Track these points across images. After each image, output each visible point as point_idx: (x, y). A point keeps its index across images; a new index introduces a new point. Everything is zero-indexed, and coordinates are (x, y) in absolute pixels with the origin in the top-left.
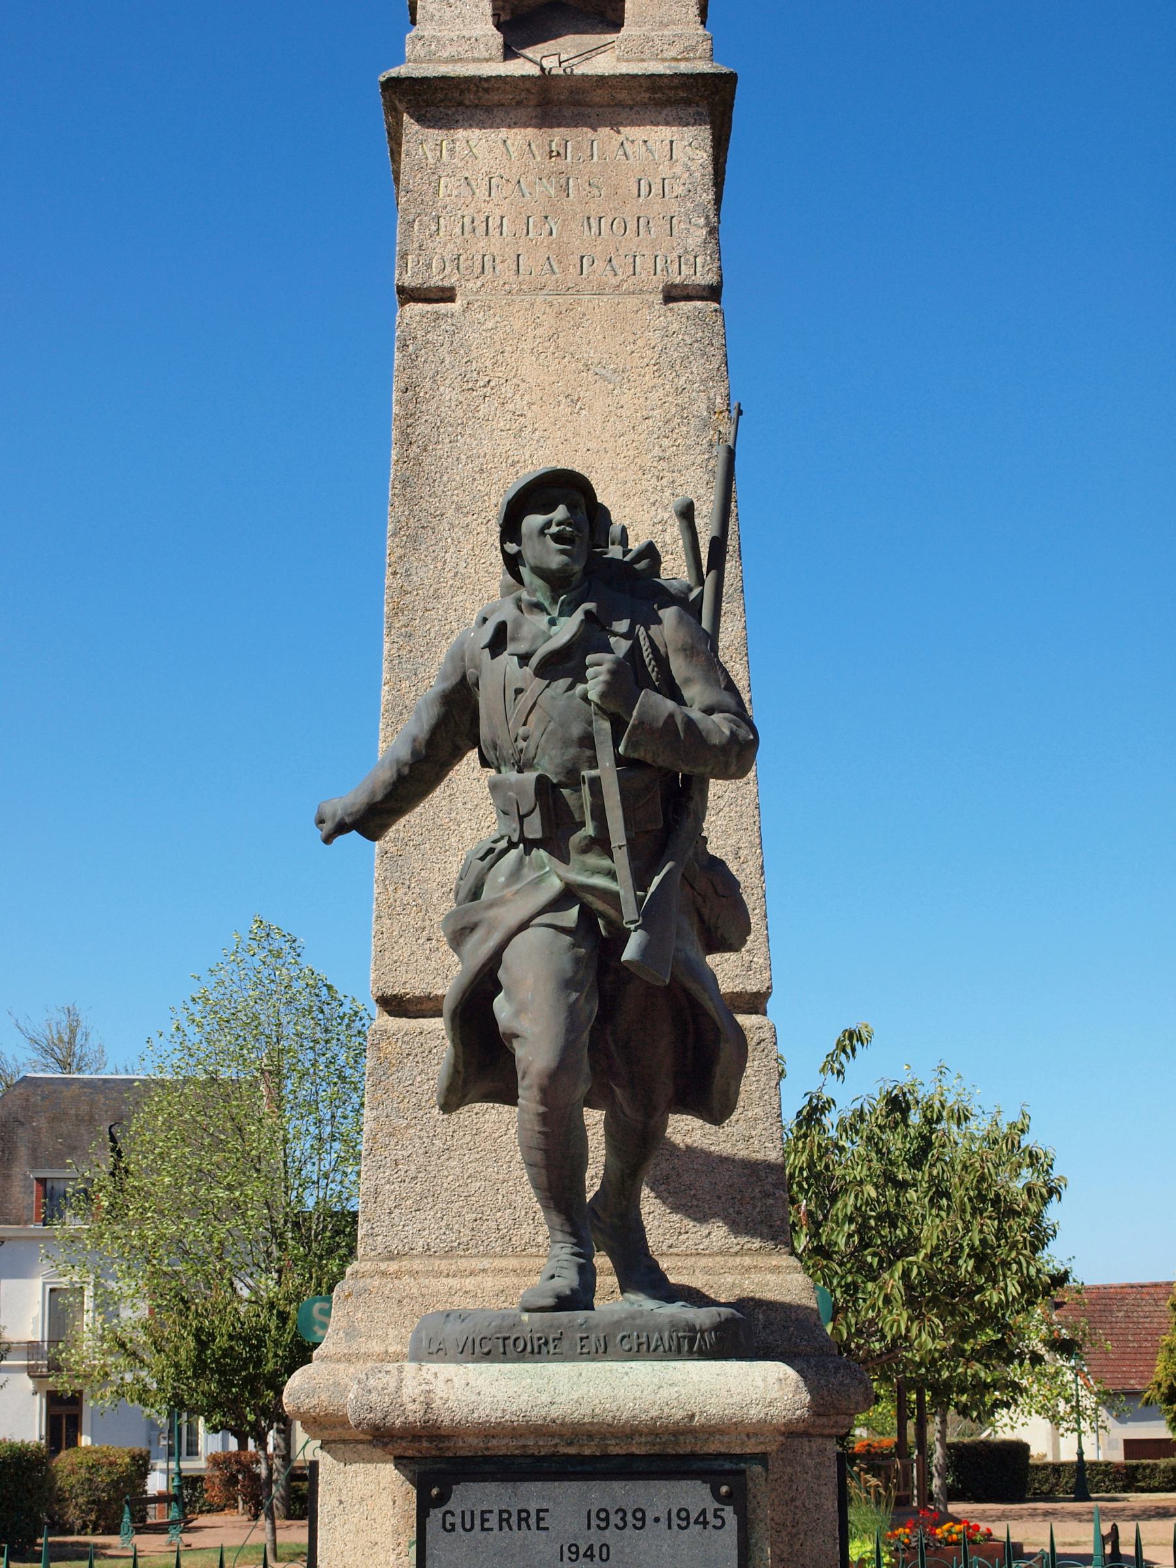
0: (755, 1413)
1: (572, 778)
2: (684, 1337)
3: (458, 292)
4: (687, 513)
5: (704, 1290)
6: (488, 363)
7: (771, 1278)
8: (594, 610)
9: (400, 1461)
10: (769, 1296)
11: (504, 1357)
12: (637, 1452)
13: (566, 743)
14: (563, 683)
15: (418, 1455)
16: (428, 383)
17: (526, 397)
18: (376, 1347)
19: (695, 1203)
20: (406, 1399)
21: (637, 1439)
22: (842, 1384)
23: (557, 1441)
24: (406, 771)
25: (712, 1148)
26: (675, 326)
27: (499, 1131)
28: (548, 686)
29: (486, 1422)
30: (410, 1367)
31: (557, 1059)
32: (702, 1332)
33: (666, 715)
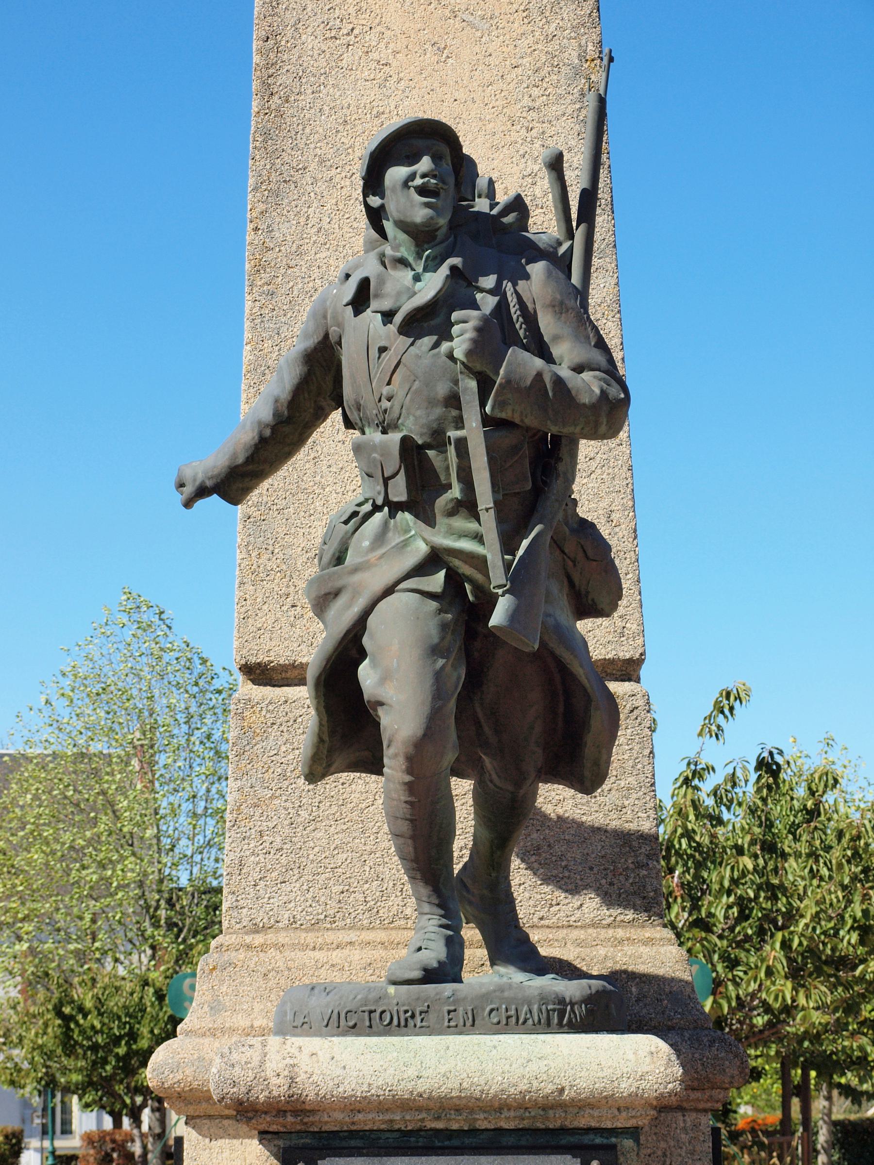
0: (626, 1087)
1: (438, 440)
2: (554, 1010)
4: (556, 165)
6: (352, 10)
7: (644, 950)
8: (460, 266)
9: (264, 1136)
11: (370, 1030)
13: (431, 403)
14: (428, 341)
15: (282, 1129)
16: (289, 32)
17: (391, 46)
18: (242, 1021)
19: (567, 874)
20: (269, 1073)
21: (506, 1113)
22: (716, 1057)
23: (424, 1115)
24: (268, 432)
25: (584, 818)
27: (365, 800)
28: (412, 344)
29: (352, 1096)
30: (274, 1041)
31: (424, 726)
32: (572, 1004)
33: (535, 373)
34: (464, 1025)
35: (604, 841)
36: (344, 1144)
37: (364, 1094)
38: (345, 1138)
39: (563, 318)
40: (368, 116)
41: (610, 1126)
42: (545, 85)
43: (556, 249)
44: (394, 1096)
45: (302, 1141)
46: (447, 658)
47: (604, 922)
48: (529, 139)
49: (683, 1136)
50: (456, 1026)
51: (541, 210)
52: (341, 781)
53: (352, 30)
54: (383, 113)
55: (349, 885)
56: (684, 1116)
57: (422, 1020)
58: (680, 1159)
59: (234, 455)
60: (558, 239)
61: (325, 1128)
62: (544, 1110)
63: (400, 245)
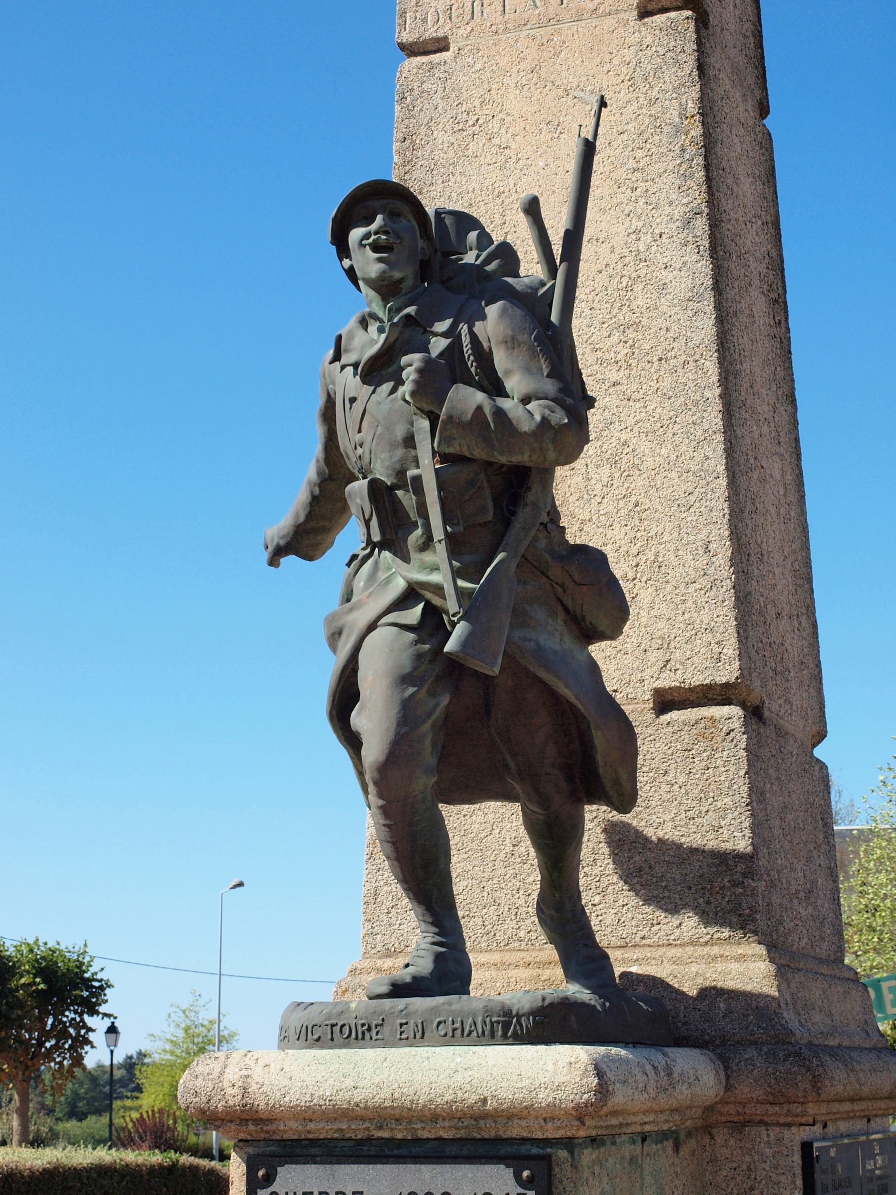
0: (544, 1097)
2: (498, 1022)
3: (451, 39)
4: (532, 208)
5: (668, 980)
6: (477, 103)
7: (734, 966)
8: (413, 314)
10: (730, 984)
12: (445, 1136)
13: (393, 446)
14: (387, 387)
15: (249, 1138)
16: (423, 130)
17: (510, 130)
19: (667, 894)
20: (226, 1084)
21: (441, 1123)
22: (788, 1072)
23: (368, 1124)
24: (317, 491)
25: (683, 840)
26: (649, 40)
28: (374, 392)
29: (297, 1106)
31: (386, 752)
32: (519, 1016)
33: (475, 407)
34: (415, 1037)
35: (702, 861)
36: (305, 1152)
37: (308, 1104)
38: (306, 1147)
39: (515, 353)
40: (491, 196)
41: (541, 1137)
42: (648, 146)
43: (537, 290)
44: (334, 1106)
45: (269, 1148)
46: (420, 687)
47: (701, 940)
48: (633, 199)
49: (767, 1150)
50: (407, 1038)
51: (644, 264)
52: (463, 813)
53: (477, 120)
54: (503, 192)
55: (470, 910)
56: (767, 1130)
57: (377, 1033)
58: (764, 1173)
59: (297, 515)
60: (542, 280)
61: (286, 1137)
62: (476, 1120)
63: (371, 302)
